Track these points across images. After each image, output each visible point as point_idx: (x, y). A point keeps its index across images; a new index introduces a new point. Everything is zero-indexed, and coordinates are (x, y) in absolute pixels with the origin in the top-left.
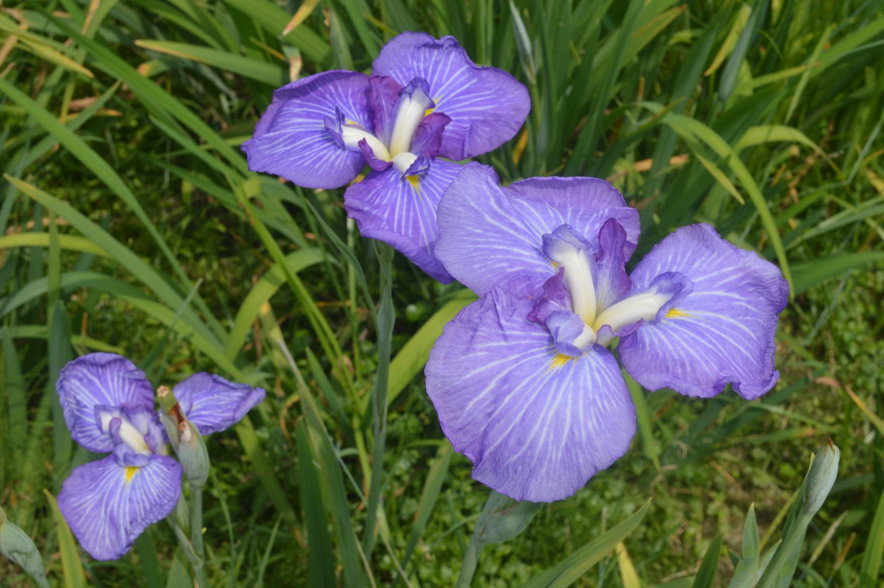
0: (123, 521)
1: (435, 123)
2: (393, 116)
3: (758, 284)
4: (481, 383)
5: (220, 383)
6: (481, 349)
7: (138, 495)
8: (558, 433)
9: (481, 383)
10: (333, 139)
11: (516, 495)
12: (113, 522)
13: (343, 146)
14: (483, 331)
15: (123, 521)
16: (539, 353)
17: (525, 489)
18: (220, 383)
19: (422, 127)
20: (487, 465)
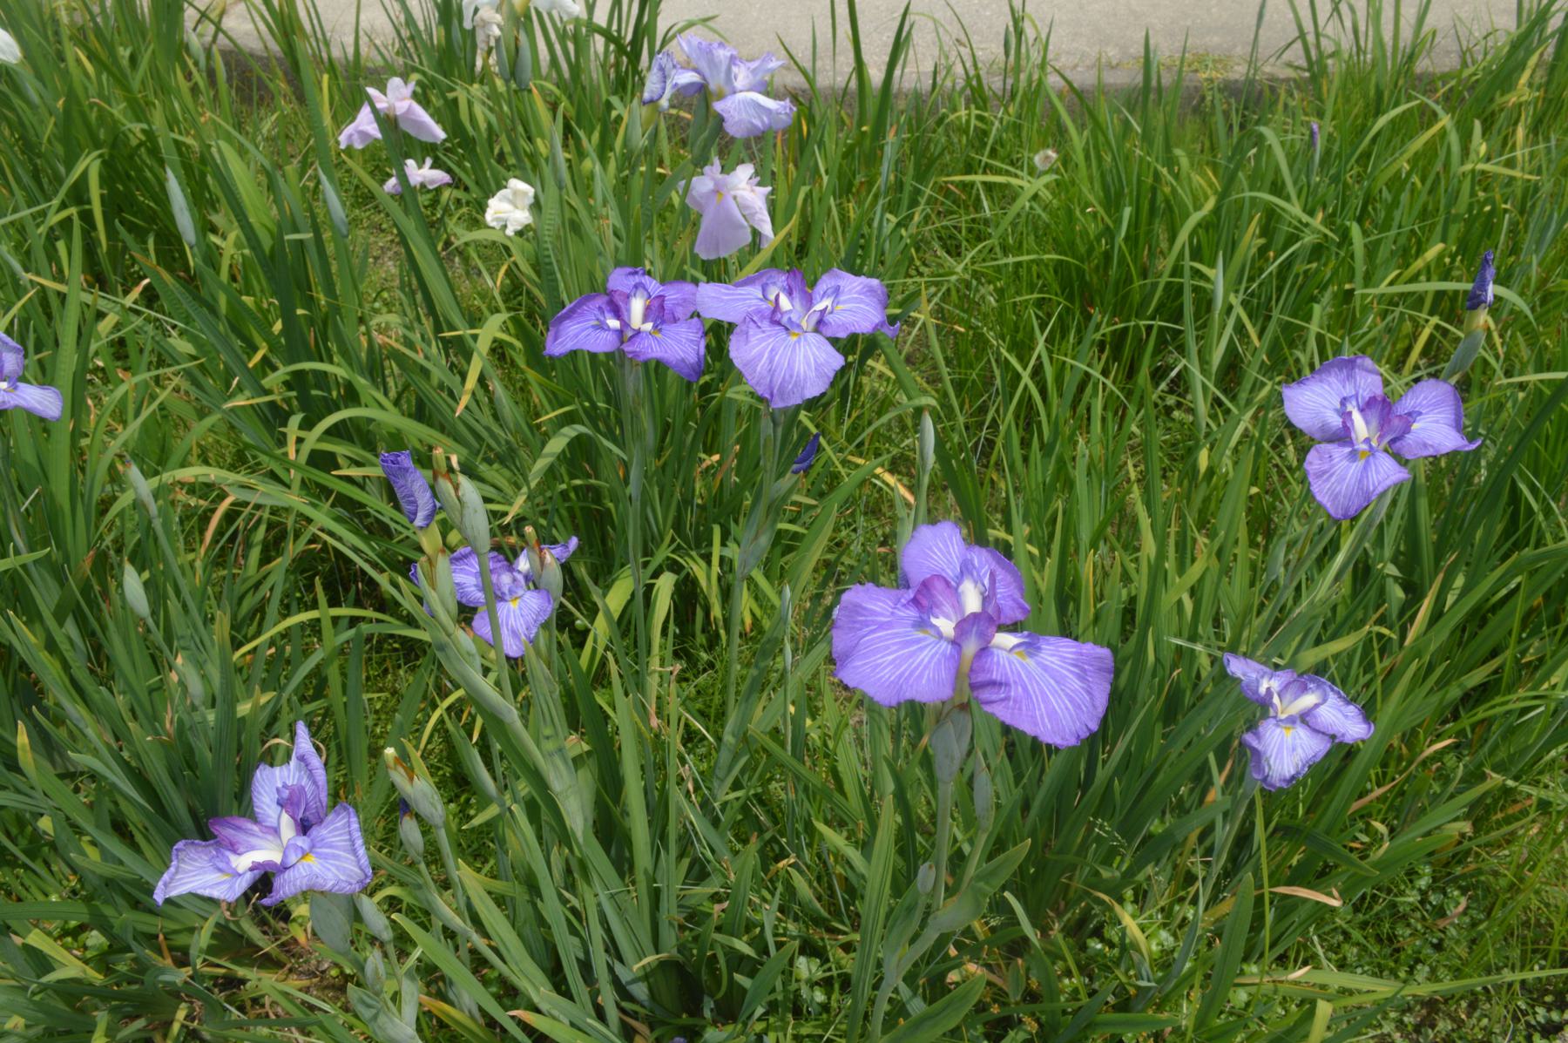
0: (522, 630)
1: (656, 303)
2: (629, 311)
3: (871, 290)
4: (761, 355)
5: (354, 852)
6: (753, 340)
7: (525, 612)
8: (808, 364)
9: (761, 355)
10: (602, 327)
11: (799, 401)
12: (515, 634)
13: (609, 329)
14: (751, 332)
15: (522, 630)
16: (783, 335)
17: (802, 395)
18: (354, 852)
19: (648, 309)
20: (776, 399)
